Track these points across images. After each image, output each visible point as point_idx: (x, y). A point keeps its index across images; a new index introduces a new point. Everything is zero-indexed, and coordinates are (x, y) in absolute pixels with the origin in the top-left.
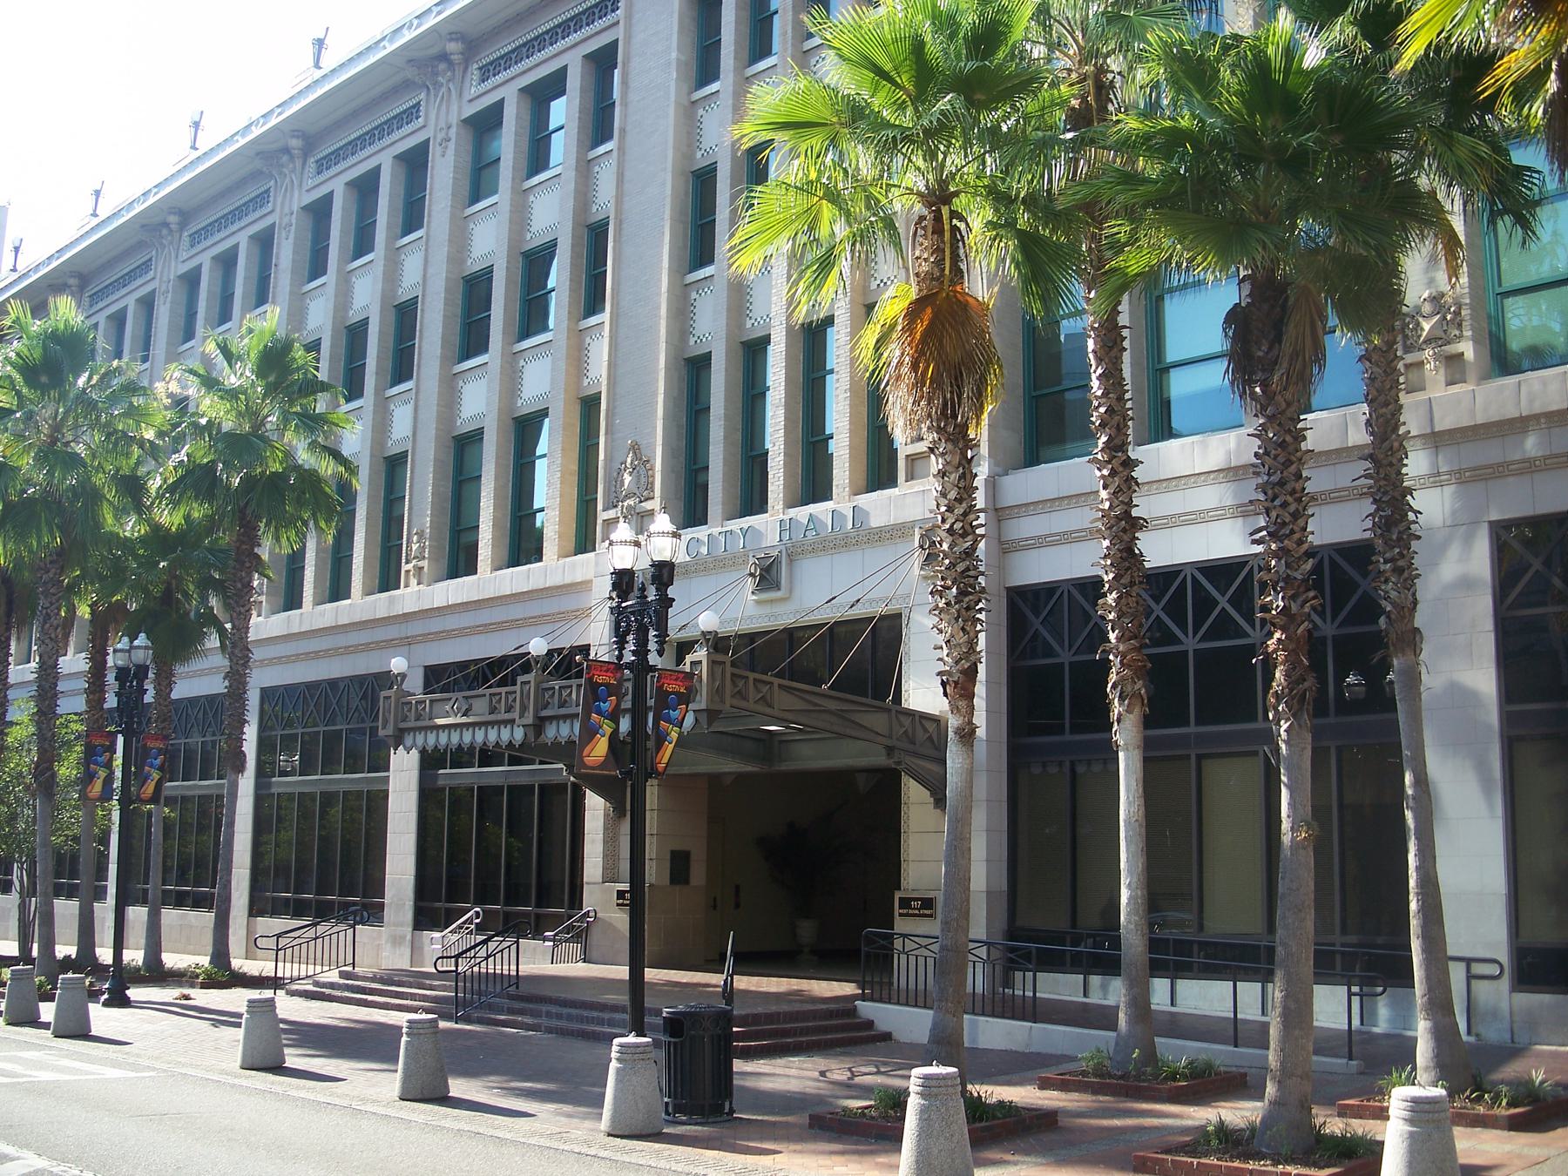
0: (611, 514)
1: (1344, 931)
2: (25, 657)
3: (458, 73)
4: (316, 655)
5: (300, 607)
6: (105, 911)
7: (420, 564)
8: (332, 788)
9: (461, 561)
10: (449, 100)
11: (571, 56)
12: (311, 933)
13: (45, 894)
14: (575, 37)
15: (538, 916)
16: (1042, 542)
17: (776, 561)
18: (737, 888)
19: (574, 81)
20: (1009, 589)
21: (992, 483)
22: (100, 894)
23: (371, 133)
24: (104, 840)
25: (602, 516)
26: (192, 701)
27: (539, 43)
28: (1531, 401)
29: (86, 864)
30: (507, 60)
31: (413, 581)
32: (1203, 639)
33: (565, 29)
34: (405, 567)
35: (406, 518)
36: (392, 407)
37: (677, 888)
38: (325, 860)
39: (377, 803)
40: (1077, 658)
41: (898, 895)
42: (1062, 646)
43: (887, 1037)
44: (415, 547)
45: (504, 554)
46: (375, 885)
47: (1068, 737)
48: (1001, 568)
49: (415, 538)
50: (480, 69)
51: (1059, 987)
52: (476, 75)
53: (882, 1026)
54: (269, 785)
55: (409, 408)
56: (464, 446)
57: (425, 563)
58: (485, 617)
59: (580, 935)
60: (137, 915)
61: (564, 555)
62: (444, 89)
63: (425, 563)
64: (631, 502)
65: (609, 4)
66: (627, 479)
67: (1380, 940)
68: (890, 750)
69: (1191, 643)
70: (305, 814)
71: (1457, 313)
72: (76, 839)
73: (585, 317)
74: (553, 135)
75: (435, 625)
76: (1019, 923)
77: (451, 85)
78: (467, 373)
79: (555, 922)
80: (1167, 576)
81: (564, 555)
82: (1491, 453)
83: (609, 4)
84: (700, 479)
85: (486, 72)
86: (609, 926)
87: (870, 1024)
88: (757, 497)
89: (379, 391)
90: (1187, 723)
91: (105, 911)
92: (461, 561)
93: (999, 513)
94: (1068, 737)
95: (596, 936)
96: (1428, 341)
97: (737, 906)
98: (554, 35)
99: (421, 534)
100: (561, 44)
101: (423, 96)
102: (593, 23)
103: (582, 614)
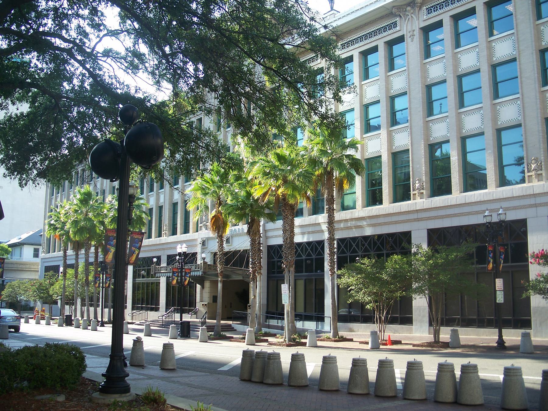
0: (201, 225)
1: (315, 312)
2: (196, 230)
3: (417, 9)
4: (151, 250)
5: (176, 234)
6: (99, 310)
7: (422, 191)
8: (149, 282)
9: (174, 233)
10: (412, 20)
11: (380, 41)
12: (139, 313)
13: (88, 305)
14: (357, 45)
15: (189, 309)
16: (272, 237)
17: (229, 237)
18: (231, 304)
19: (356, 59)
20: (268, 246)
21: (264, 225)
22: (98, 306)
23: (366, 36)
24: (99, 294)
25: (200, 225)
26: (144, 258)
27: (370, 35)
28: (434, 204)
29: (95, 299)
30: (352, 42)
31: (165, 236)
32: (400, 250)
33: (379, 31)
34: (163, 232)
35: (411, 173)
36: (394, 134)
37: (214, 303)
38: (147, 299)
39: (158, 284)
40: (340, 255)
41: (248, 305)
42: (397, 247)
43: (236, 330)
44: (165, 228)
45: (183, 230)
46: (158, 303)
47: (276, 275)
48: (266, 242)
49: (417, 182)
50: (427, 9)
51: (273, 322)
52: (425, 12)
53: (235, 328)
54: (135, 281)
55: (163, 195)
56: (175, 205)
57: (167, 232)
58: (394, 219)
59: (196, 313)
60: (85, 308)
61: (364, 207)
62: (410, 16)
63: (167, 232)
64: (204, 223)
65: (450, 2)
66: (204, 218)
67: (320, 314)
68: (243, 277)
69: (314, 257)
70: (148, 286)
71: (541, 163)
72: (93, 293)
73: (391, 127)
74: (494, 22)
75: (169, 246)
76: (269, 310)
77: (413, 15)
78: (436, 120)
79: (191, 310)
80: (299, 244)
81: (364, 207)
82: (374, 221)
83: (450, 2)
84: (175, 227)
85: (429, 11)
86: (201, 311)
87: (233, 328)
88: (175, 232)
89: (157, 191)
90: (303, 273)
91: (99, 310)
92: (174, 233)
93: (265, 231)
94: (276, 275)
95: (199, 313)
96: (533, 170)
97: (231, 307)
98: (375, 33)
99: (166, 225)
100: (351, 48)
101: (398, 19)
102: (454, 3)
103: (196, 246)
